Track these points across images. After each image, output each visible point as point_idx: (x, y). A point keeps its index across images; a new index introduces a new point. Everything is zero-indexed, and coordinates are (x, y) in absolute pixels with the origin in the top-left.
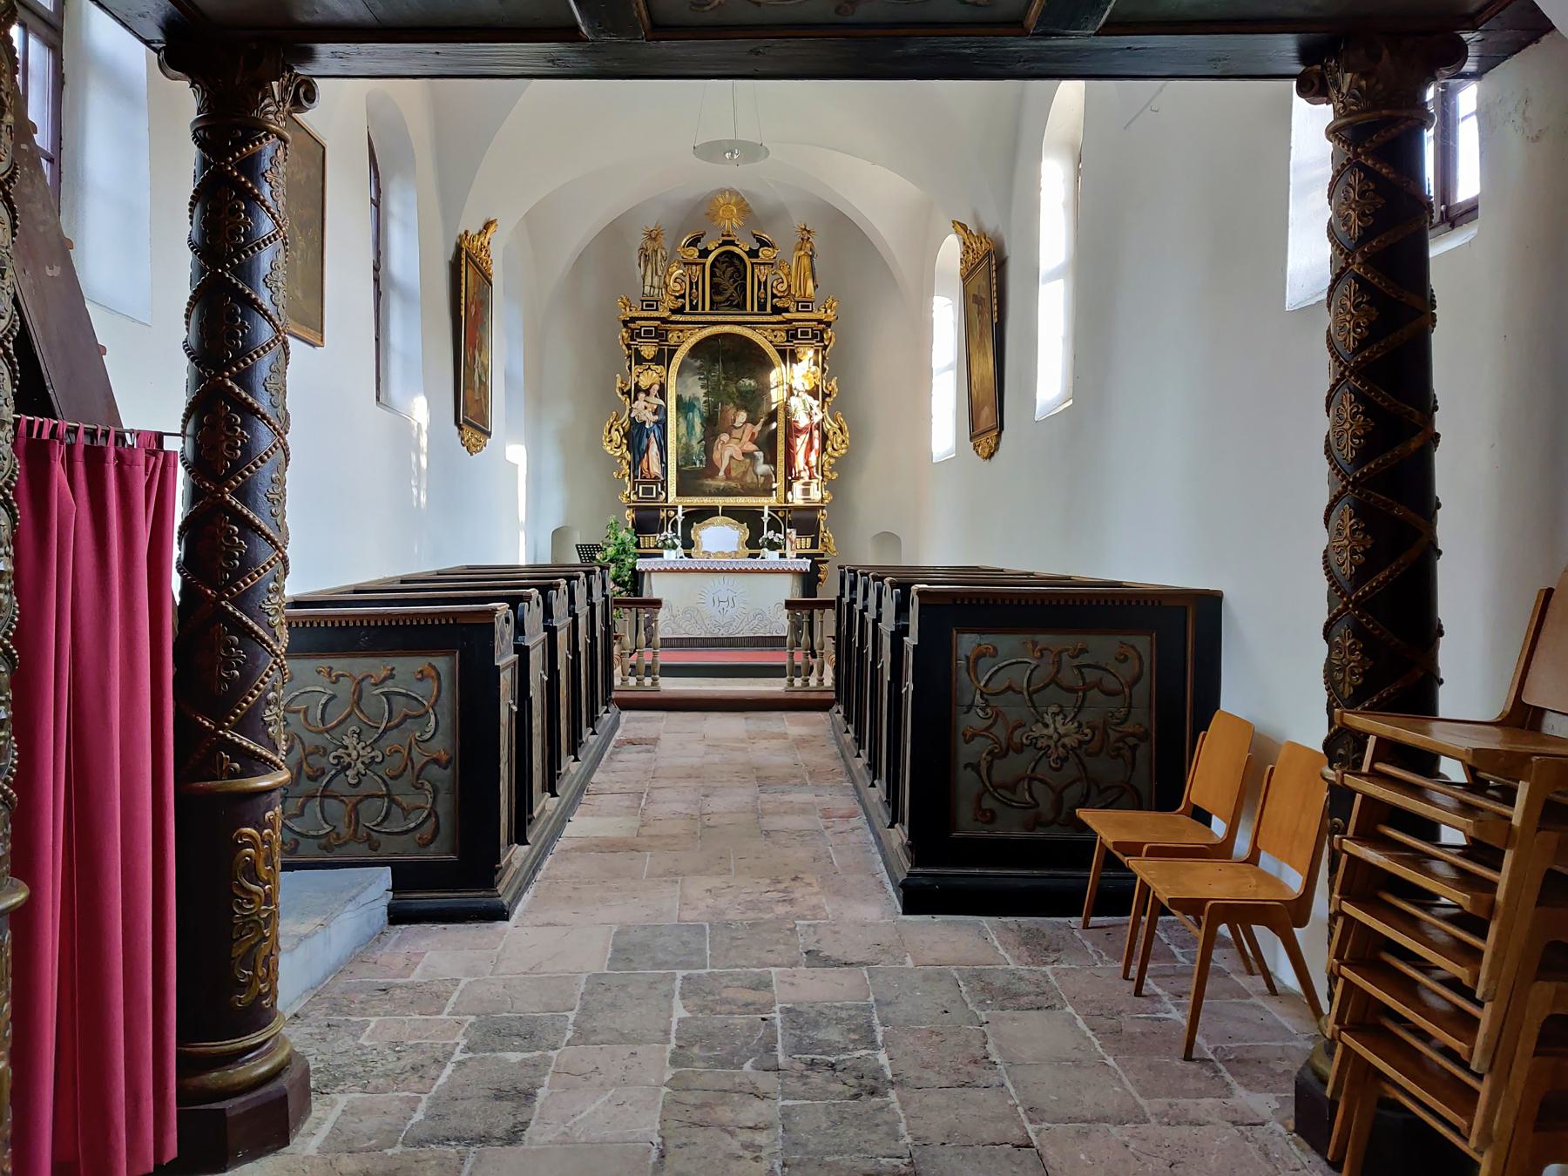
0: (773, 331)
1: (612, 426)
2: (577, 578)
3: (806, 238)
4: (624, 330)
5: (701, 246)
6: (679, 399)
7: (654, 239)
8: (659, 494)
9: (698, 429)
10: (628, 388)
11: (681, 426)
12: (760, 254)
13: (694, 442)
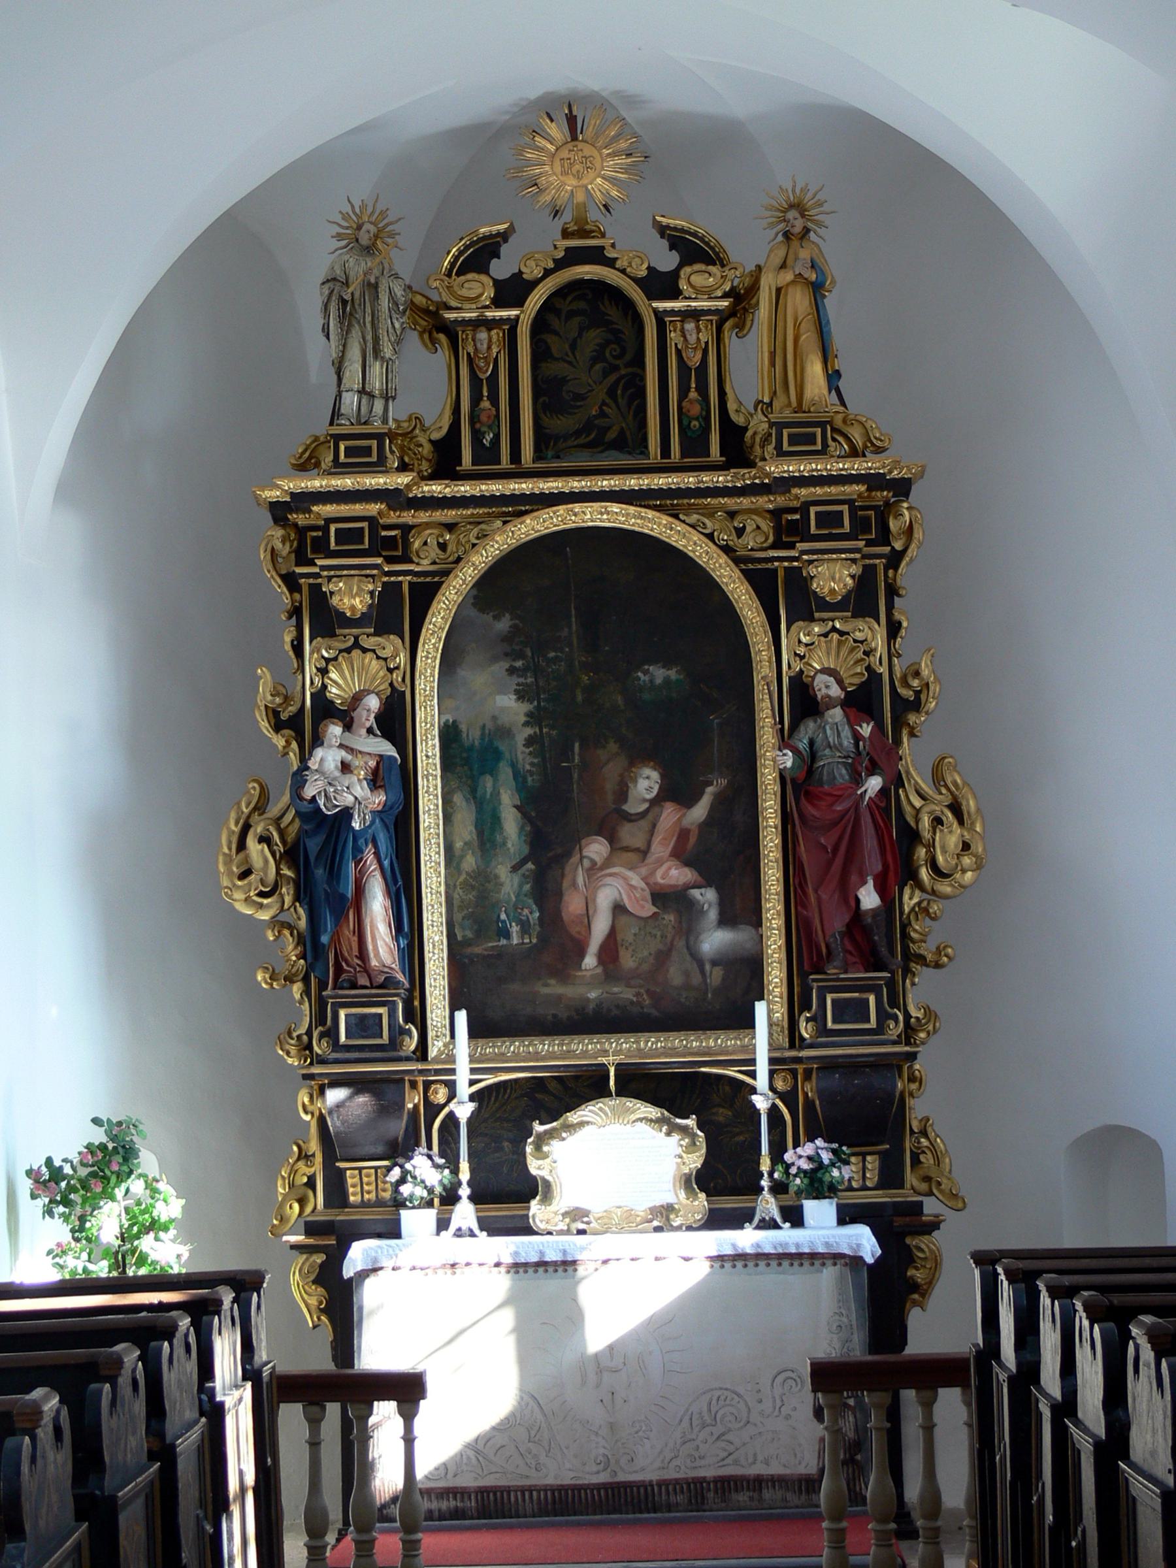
0: (732, 515)
1: (246, 828)
2: (169, 1333)
3: (798, 229)
4: (279, 532)
5: (501, 268)
6: (449, 736)
7: (369, 250)
8: (398, 1034)
9: (511, 824)
10: (293, 709)
11: (458, 817)
12: (683, 285)
13: (503, 871)
